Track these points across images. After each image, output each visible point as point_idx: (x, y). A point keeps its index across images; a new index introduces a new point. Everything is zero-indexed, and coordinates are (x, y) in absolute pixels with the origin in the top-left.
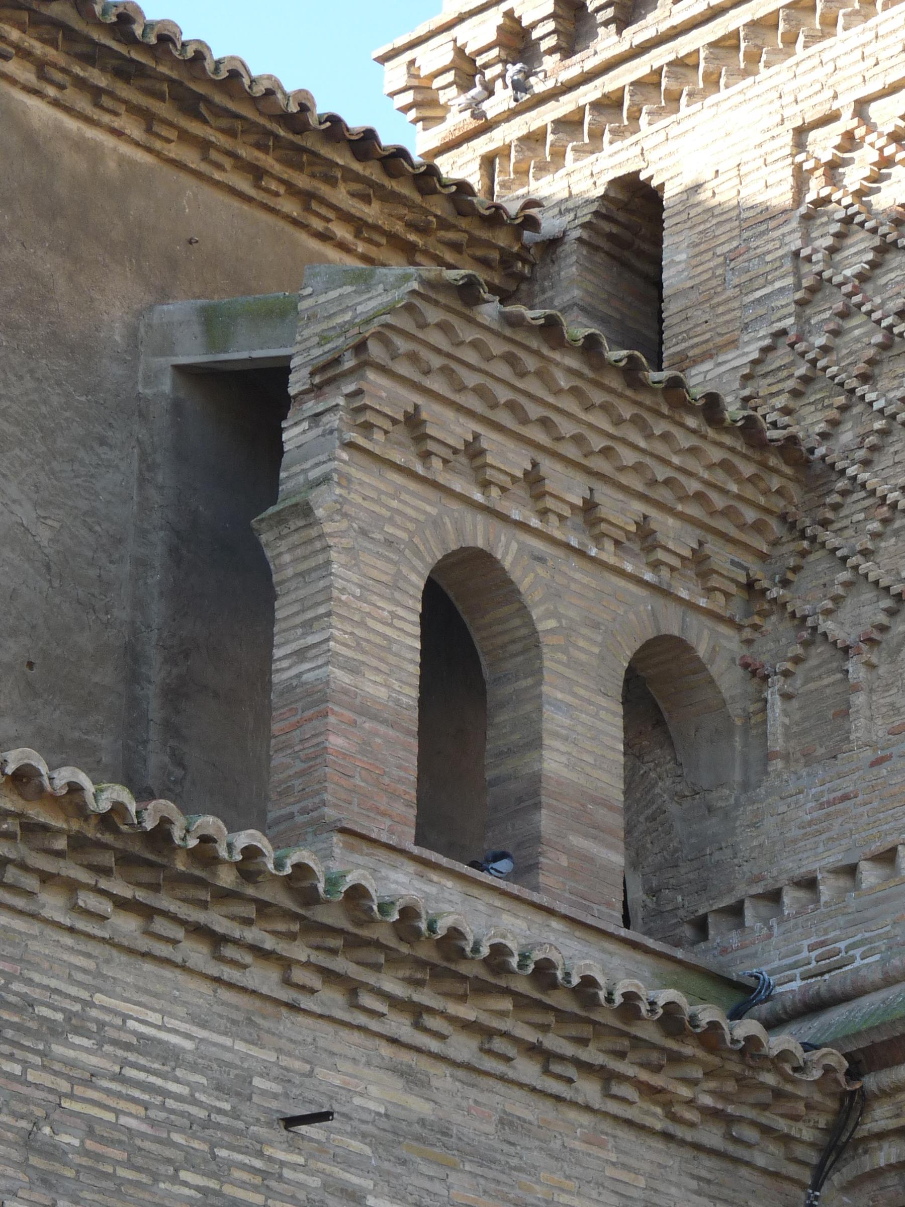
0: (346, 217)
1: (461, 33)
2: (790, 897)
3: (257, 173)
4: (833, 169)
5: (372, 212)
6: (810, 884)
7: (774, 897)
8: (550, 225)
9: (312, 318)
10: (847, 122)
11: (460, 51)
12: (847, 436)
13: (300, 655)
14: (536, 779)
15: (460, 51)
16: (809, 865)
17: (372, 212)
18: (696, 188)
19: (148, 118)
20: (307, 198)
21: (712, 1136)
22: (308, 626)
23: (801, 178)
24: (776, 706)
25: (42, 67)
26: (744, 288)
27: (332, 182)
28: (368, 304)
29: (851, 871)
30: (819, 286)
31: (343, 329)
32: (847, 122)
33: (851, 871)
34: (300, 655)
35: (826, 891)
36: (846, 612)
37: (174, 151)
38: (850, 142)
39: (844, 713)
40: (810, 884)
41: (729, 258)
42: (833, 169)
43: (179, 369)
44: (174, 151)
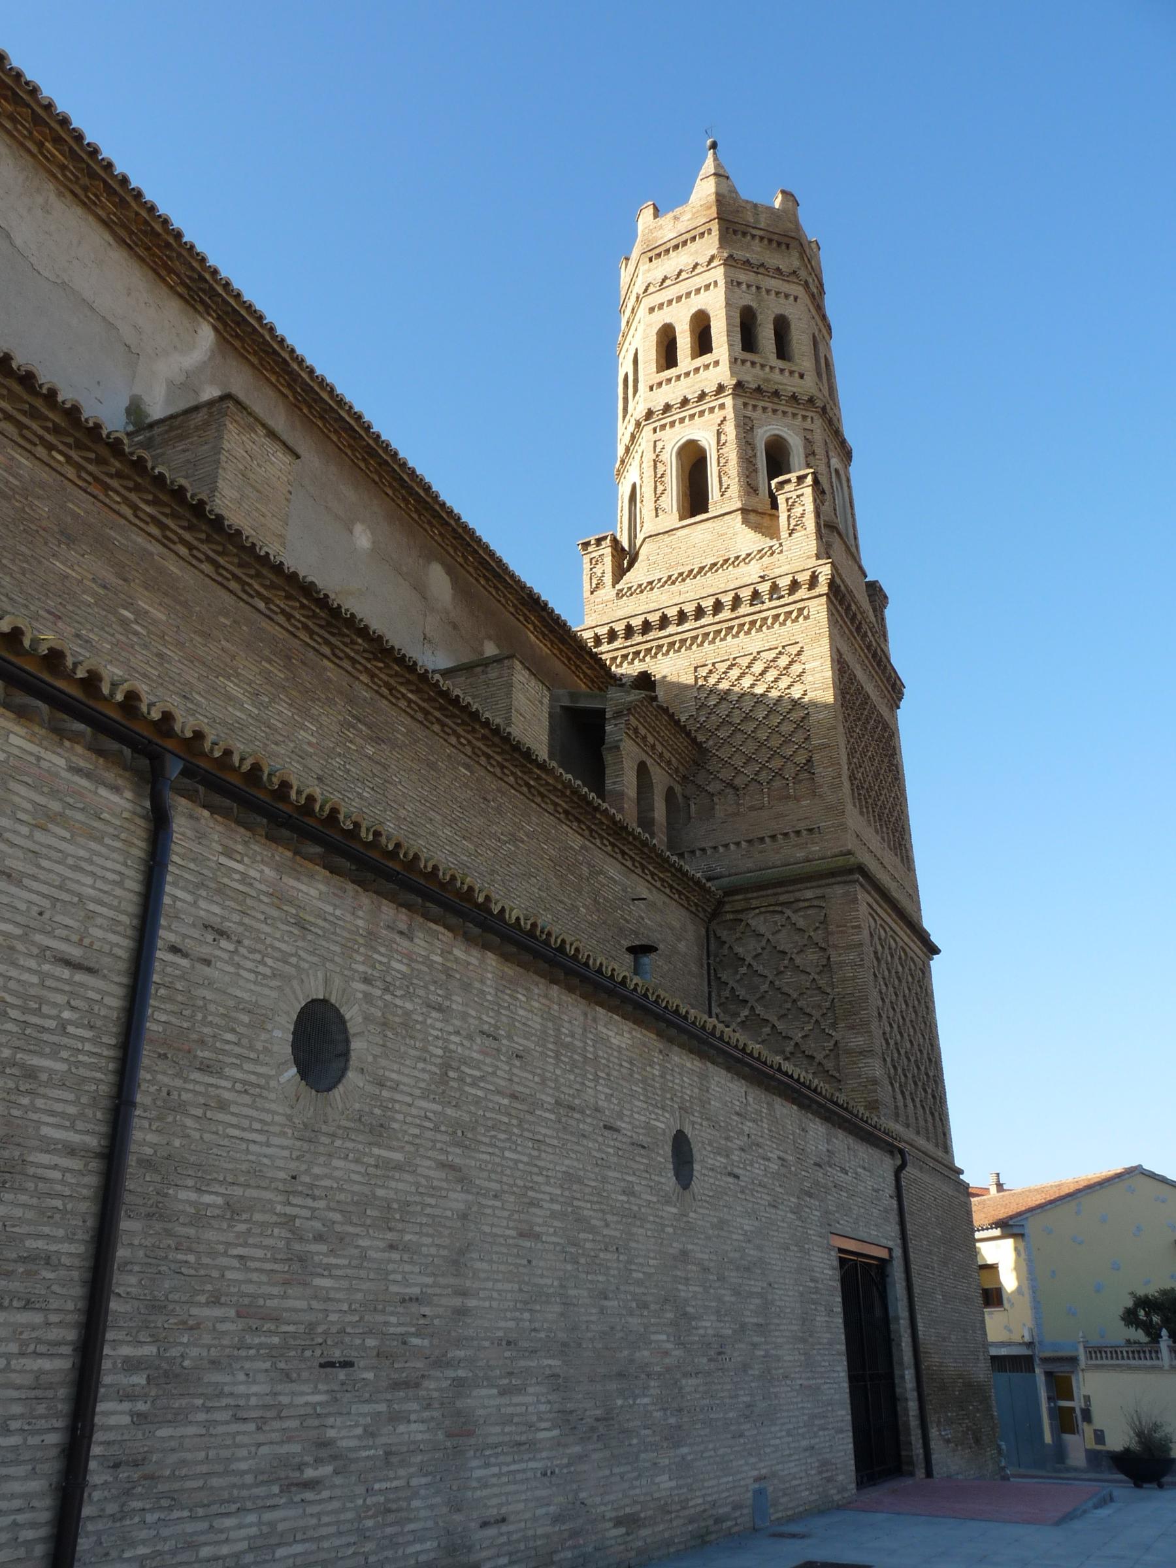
0: (584, 673)
1: (597, 630)
2: (698, 853)
3: (569, 659)
4: (706, 678)
5: (589, 672)
6: (703, 850)
7: (693, 852)
8: (624, 680)
9: (611, 699)
10: (710, 667)
11: (596, 634)
12: (711, 743)
13: (614, 783)
14: (653, 819)
15: (596, 634)
16: (704, 845)
17: (589, 672)
18: (665, 677)
19: (552, 643)
20: (577, 666)
21: (693, 909)
22: (617, 776)
23: (696, 678)
24: (693, 806)
25: (535, 627)
26: (682, 703)
27: (583, 663)
28: (629, 699)
29: (715, 848)
30: (703, 705)
31: (623, 704)
32: (710, 667)
33: (715, 848)
34: (614, 783)
35: (709, 852)
36: (712, 785)
37: (555, 651)
38: (711, 672)
39: (713, 809)
40: (726, 846)
41: (676, 695)
42: (706, 678)
43: (562, 707)
44: (555, 651)
